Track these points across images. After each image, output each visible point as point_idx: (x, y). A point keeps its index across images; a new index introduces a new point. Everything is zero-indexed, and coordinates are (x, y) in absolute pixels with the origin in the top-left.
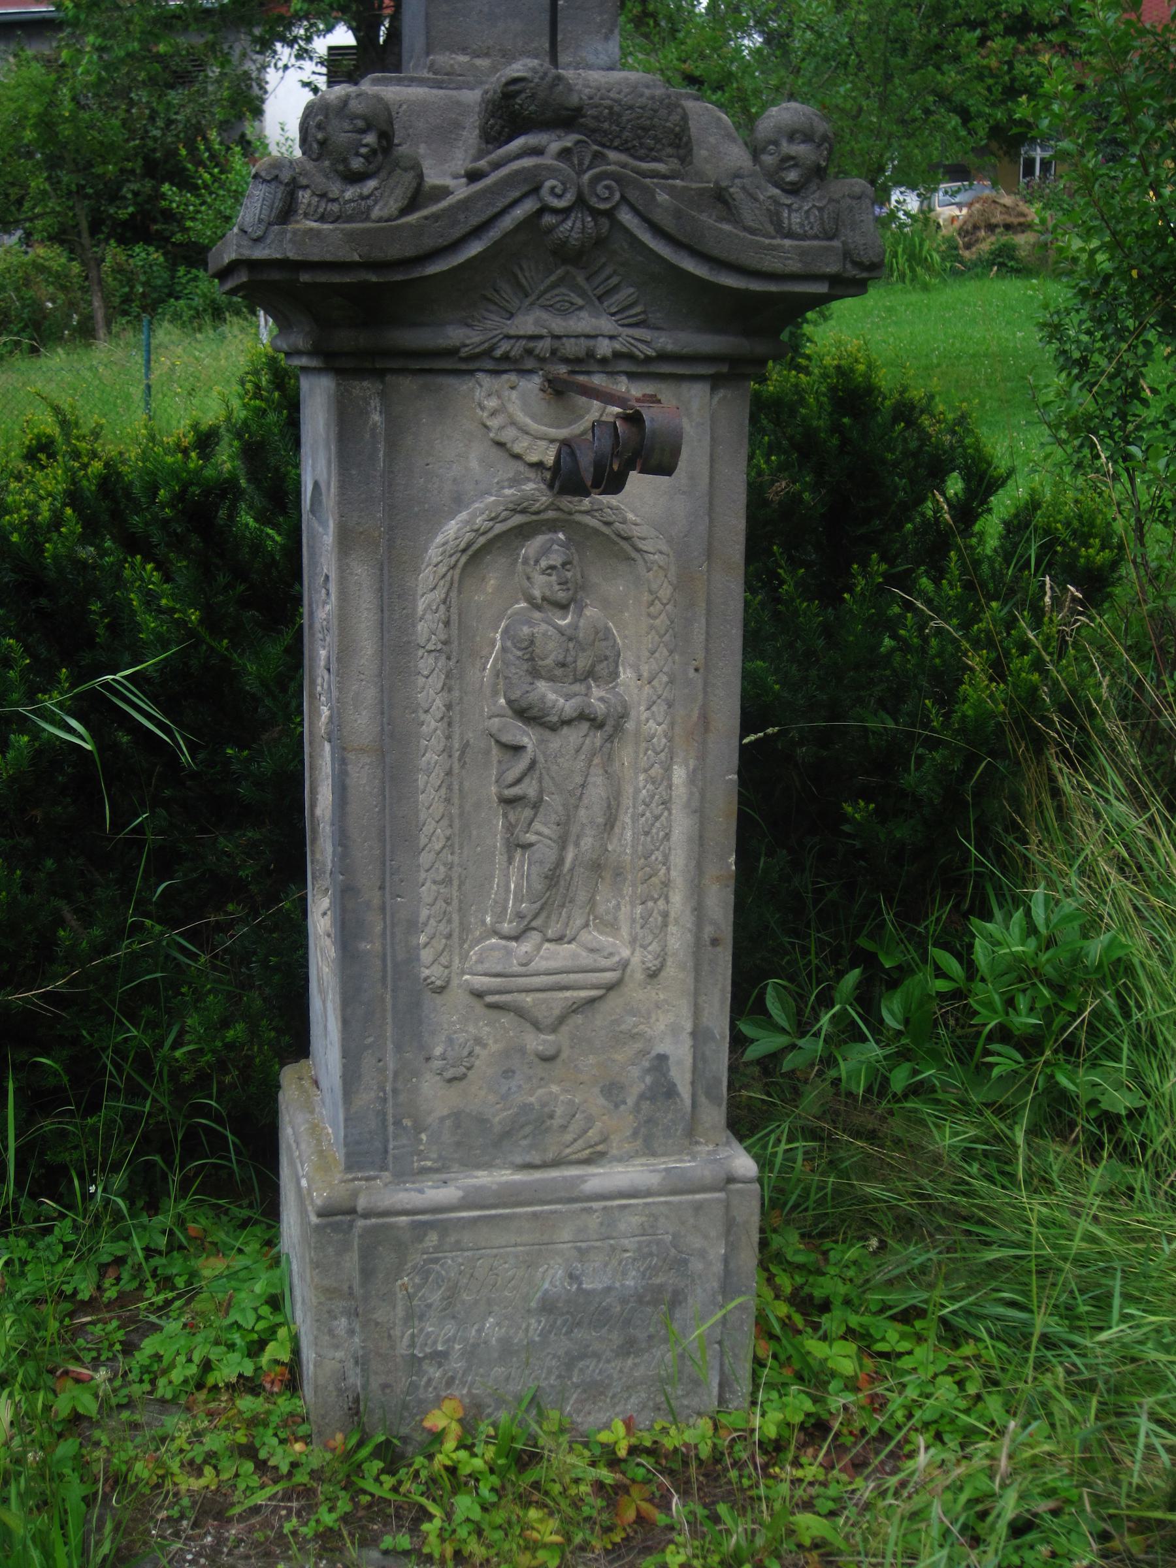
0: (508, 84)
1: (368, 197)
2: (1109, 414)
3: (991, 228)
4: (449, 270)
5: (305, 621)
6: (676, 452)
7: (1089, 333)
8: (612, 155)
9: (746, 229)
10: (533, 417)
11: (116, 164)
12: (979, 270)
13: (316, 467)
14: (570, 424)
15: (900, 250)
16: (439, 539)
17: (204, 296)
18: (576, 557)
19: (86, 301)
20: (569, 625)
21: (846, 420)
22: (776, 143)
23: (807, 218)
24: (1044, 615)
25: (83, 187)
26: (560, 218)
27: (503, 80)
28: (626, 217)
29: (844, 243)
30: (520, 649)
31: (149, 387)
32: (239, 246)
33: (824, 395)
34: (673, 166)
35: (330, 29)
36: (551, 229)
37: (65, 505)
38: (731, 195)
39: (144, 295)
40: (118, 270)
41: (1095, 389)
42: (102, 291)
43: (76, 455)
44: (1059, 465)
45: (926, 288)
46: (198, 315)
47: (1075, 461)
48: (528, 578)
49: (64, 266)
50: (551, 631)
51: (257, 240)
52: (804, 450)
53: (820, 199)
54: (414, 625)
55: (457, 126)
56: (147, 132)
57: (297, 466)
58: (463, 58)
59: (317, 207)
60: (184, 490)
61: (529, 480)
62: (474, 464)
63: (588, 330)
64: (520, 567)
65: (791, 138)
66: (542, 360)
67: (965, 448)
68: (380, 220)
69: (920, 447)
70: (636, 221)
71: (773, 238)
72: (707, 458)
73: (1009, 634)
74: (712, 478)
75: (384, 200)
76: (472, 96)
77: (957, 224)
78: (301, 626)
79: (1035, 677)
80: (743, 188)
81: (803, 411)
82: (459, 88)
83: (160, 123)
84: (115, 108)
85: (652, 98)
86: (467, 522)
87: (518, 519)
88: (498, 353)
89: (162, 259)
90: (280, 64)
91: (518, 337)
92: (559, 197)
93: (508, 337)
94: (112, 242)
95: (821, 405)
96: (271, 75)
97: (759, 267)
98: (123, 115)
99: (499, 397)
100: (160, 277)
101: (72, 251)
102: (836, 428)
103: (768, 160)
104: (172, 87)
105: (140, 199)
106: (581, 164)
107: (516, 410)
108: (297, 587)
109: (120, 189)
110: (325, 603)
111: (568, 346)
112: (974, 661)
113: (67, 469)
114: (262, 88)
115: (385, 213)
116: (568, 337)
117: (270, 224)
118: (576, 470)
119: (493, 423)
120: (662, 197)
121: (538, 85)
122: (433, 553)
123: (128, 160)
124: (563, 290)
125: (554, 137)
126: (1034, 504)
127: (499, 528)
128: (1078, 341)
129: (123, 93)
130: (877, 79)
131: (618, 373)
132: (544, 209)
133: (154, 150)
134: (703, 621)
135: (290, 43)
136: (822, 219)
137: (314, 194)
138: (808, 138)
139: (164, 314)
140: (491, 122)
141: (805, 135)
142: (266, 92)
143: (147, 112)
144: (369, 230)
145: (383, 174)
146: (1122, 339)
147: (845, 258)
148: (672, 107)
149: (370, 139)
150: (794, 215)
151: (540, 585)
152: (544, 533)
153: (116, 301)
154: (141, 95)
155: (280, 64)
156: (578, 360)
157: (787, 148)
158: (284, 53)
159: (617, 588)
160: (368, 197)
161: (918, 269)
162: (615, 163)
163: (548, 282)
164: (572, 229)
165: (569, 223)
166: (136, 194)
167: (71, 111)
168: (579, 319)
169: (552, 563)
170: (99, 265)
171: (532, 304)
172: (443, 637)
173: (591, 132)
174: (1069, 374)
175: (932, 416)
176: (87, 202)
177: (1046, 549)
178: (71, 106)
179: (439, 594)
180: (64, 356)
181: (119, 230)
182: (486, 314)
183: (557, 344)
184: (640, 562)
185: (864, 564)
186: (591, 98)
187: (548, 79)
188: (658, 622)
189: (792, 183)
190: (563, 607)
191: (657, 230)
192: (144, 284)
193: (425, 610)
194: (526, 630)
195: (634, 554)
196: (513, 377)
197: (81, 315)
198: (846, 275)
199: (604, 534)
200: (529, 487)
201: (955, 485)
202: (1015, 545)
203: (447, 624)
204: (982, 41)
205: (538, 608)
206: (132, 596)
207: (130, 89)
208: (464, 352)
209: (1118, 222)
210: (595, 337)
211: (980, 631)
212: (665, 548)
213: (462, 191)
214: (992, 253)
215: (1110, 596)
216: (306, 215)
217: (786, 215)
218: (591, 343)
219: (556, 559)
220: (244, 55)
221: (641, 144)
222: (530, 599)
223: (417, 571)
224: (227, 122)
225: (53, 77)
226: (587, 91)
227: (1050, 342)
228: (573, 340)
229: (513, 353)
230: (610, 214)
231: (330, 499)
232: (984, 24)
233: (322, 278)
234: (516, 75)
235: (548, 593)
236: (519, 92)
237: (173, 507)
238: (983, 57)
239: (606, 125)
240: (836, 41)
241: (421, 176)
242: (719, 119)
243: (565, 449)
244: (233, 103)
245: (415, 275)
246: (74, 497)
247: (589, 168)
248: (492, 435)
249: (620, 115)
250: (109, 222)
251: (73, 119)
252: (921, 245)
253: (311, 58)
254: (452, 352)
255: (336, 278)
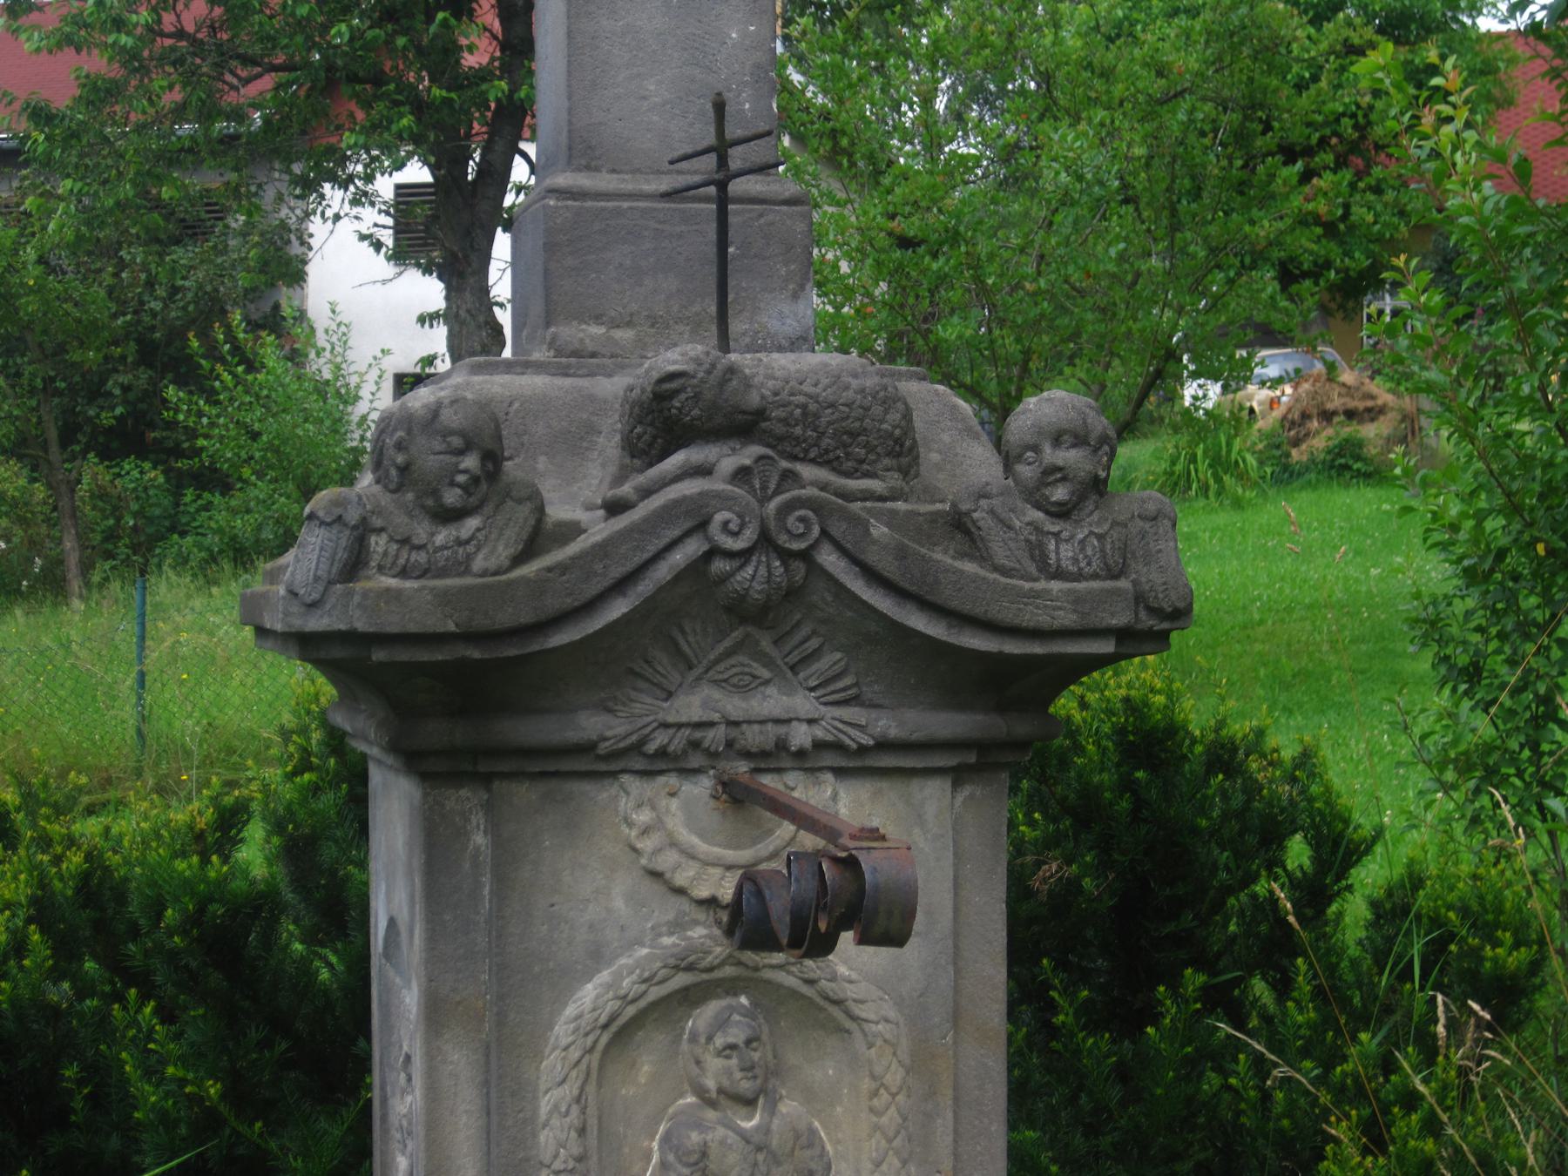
0: (661, 381)
1: (468, 542)
2: (1514, 744)
3: (1327, 416)
4: (581, 641)
5: (376, 1094)
6: (909, 915)
7: (1480, 629)
8: (807, 471)
9: (997, 569)
10: (702, 836)
11: (98, 350)
12: (1313, 476)
13: (392, 896)
14: (754, 842)
15: (1200, 452)
16: (570, 1011)
17: (220, 531)
18: (766, 1029)
19: (52, 539)
20: (757, 1128)
21: (1140, 774)
22: (1036, 448)
23: (1083, 549)
24: (1437, 1053)
25: (52, 380)
26: (736, 563)
27: (655, 375)
28: (829, 559)
29: (1135, 583)
30: (688, 1165)
31: (142, 676)
32: (286, 614)
33: (1108, 737)
34: (892, 483)
35: (399, 166)
36: (724, 579)
37: (29, 920)
38: (974, 522)
39: (135, 529)
40: (101, 495)
41: (1493, 710)
42: (76, 525)
43: (44, 842)
44: (1447, 820)
45: (1238, 504)
46: (213, 559)
47: (1469, 815)
48: (698, 1062)
49: (23, 490)
50: (732, 1138)
51: (313, 605)
52: (1082, 816)
53: (1098, 524)
54: (535, 1135)
55: (591, 430)
56: (142, 303)
57: (363, 865)
58: (597, 330)
59: (397, 556)
60: (201, 909)
61: (696, 923)
62: (619, 903)
63: (778, 712)
64: (685, 1046)
65: (1057, 441)
66: (713, 755)
67: (1311, 800)
68: (484, 574)
69: (1249, 801)
70: (843, 563)
71: (1036, 580)
72: (949, 884)
73: (1387, 1080)
74: (956, 910)
75: (488, 545)
76: (613, 387)
77: (1277, 413)
78: (370, 1101)
79: (1429, 1146)
80: (992, 512)
81: (1080, 761)
82: (591, 375)
83: (161, 292)
84: (99, 271)
85: (862, 391)
86: (609, 986)
87: (682, 980)
88: (651, 747)
89: (161, 479)
90: (329, 213)
91: (680, 726)
92: (735, 534)
93: (665, 725)
94: (91, 455)
95: (1103, 751)
96: (316, 227)
97: (1017, 621)
98: (109, 281)
99: (653, 808)
100: (158, 505)
101: (34, 468)
102: (1127, 785)
103: (1026, 471)
104: (177, 242)
105: (131, 396)
106: (764, 488)
107: (676, 823)
108: (362, 1043)
109: (103, 382)
110: (404, 1092)
111: (749, 735)
112: (1339, 1130)
113: (34, 867)
114: (303, 243)
115: (492, 564)
116: (749, 722)
117: (331, 583)
118: (764, 917)
119: (646, 845)
120: (879, 530)
121: (702, 381)
122: (562, 1031)
123: (116, 343)
124: (741, 658)
125: (726, 450)
126: (1415, 881)
127: (655, 993)
128: (1465, 642)
129: (111, 251)
130: (1160, 233)
131: (820, 769)
132: (714, 552)
133: (153, 328)
134: (950, 1115)
135: (344, 185)
136: (1102, 550)
137: (391, 539)
138: (1079, 439)
139: (162, 557)
140: (639, 430)
141: (1076, 436)
142: (310, 248)
143: (143, 276)
144: (468, 590)
145: (488, 509)
146: (1527, 637)
147: (1137, 603)
148: (890, 400)
149: (471, 462)
150: (1063, 547)
151: (715, 1073)
152: (718, 997)
153: (97, 538)
154: (135, 254)
155: (329, 213)
156: (764, 754)
157: (1052, 456)
158: (335, 196)
159: (824, 1070)
160: (468, 542)
161: (1226, 478)
162: (812, 484)
163: (721, 648)
164: (753, 578)
165: (750, 570)
166: (126, 389)
167: (36, 278)
168: (765, 697)
169: (731, 1040)
170: (73, 491)
171: (699, 679)
172: (576, 1151)
173: (774, 441)
174: (1454, 690)
175: (1263, 756)
176: (56, 400)
177: (1436, 950)
178: (38, 270)
179: (570, 1090)
180: (21, 620)
181: (101, 439)
182: (633, 694)
183: (734, 732)
184: (857, 1035)
185: (1174, 985)
186: (776, 394)
187: (718, 372)
188: (884, 1120)
189: (1059, 504)
190: (749, 1102)
191: (872, 575)
192: (136, 515)
193: (550, 1113)
194: (695, 1137)
195: (848, 1024)
196: (672, 780)
197: (46, 557)
198: (1139, 626)
199: (803, 996)
200: (698, 933)
201: (1298, 854)
202: (1390, 940)
203: (582, 1131)
204: (1307, 176)
205: (713, 1104)
206: (124, 1055)
207: (120, 244)
208: (603, 748)
209: (1513, 478)
210: (789, 721)
211: (1345, 1074)
212: (892, 1014)
213: (599, 529)
214: (1329, 452)
215: (1530, 1014)
216: (380, 568)
217: (1052, 547)
218: (782, 730)
219: (737, 1035)
220: (280, 198)
221: (847, 454)
222: (701, 1092)
223: (538, 1056)
224: (254, 289)
225: (14, 232)
226: (771, 383)
227: (1424, 645)
228: (756, 727)
229: (671, 748)
230: (806, 556)
231: (414, 947)
232: (1309, 152)
233: (403, 655)
234: (672, 368)
235: (726, 1083)
236: (677, 392)
237: (184, 933)
238: (1307, 200)
239: (798, 430)
240: (1101, 183)
241: (540, 510)
242: (955, 407)
243: (747, 887)
244: (264, 266)
245: (535, 647)
246: (42, 909)
247: (776, 493)
248: (644, 861)
249: (817, 416)
250: (87, 429)
251: (39, 289)
252: (1229, 445)
253: (372, 204)
254: (585, 749)
255: (424, 655)
